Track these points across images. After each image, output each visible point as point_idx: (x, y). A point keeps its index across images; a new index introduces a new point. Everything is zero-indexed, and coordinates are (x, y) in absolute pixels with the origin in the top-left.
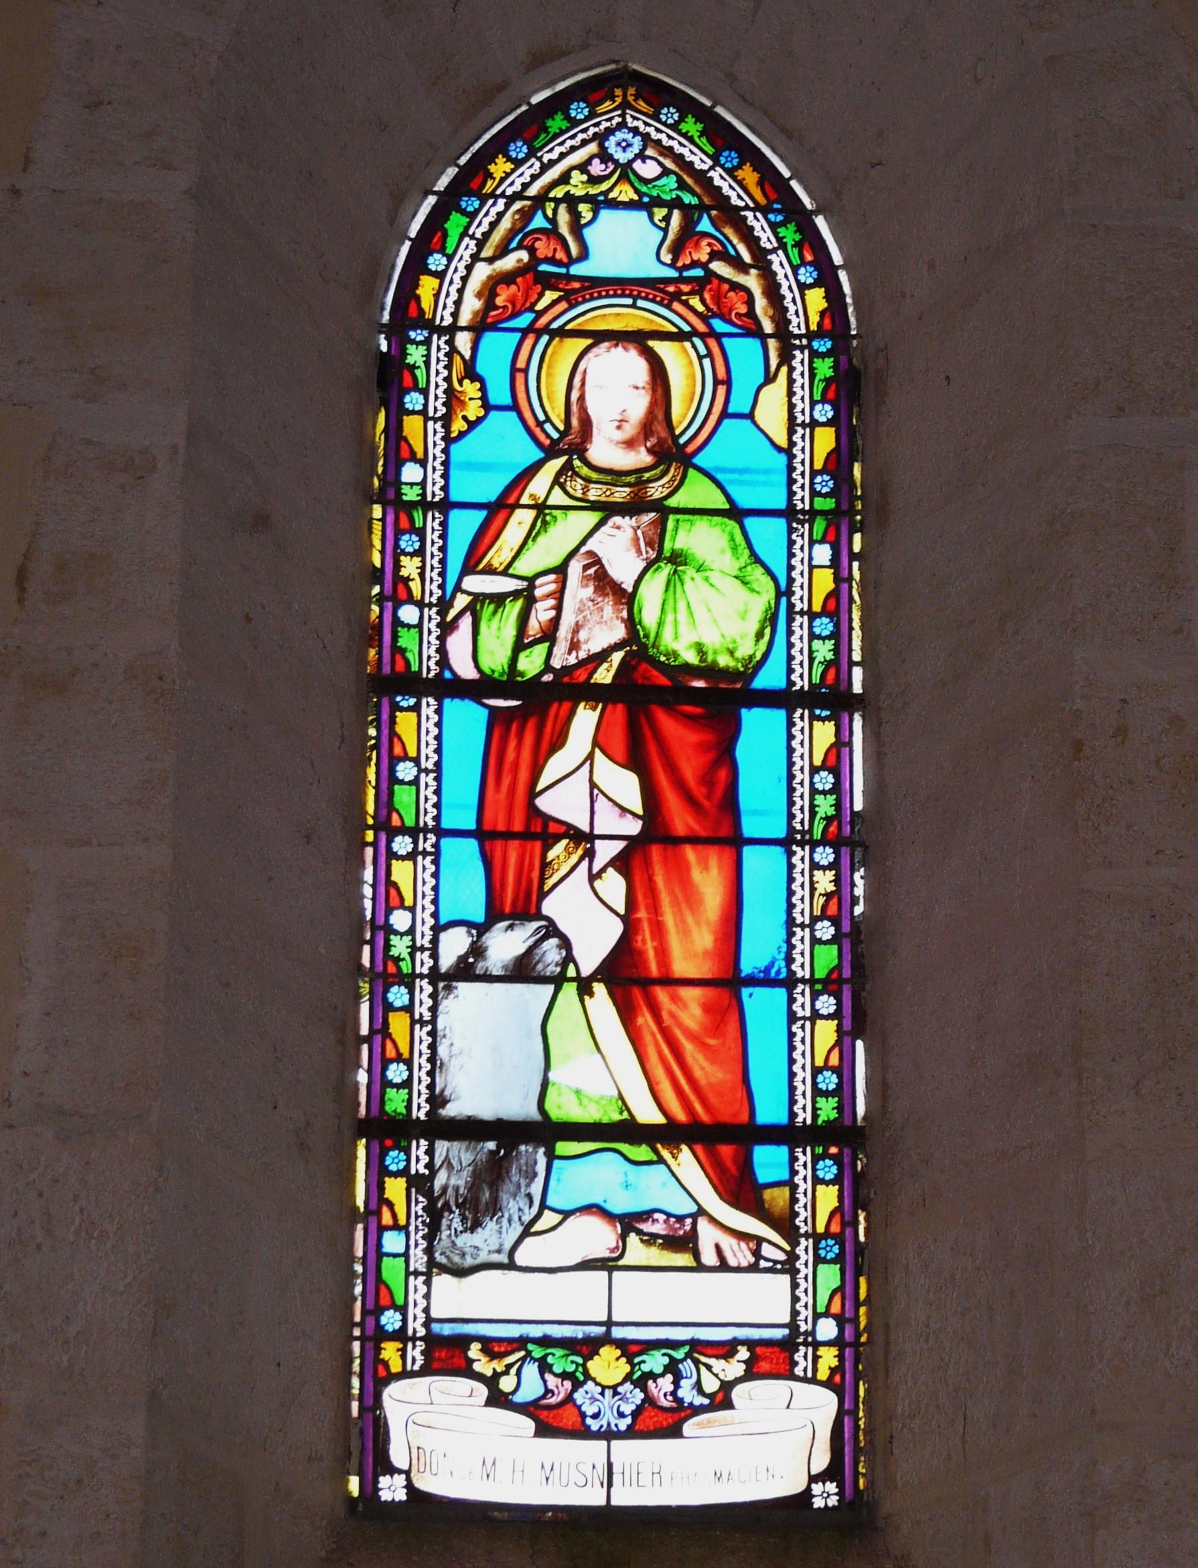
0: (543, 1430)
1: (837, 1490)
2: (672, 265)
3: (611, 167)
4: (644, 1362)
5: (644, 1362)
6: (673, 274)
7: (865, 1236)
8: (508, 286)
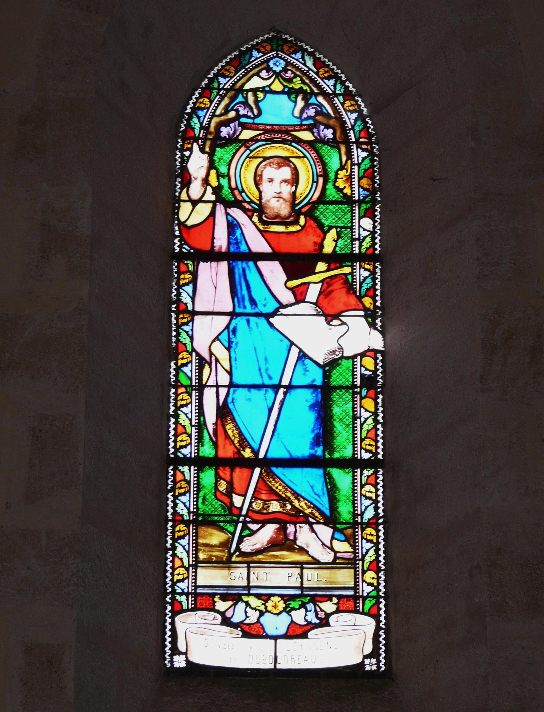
0: (246, 635)
5: (290, 604)
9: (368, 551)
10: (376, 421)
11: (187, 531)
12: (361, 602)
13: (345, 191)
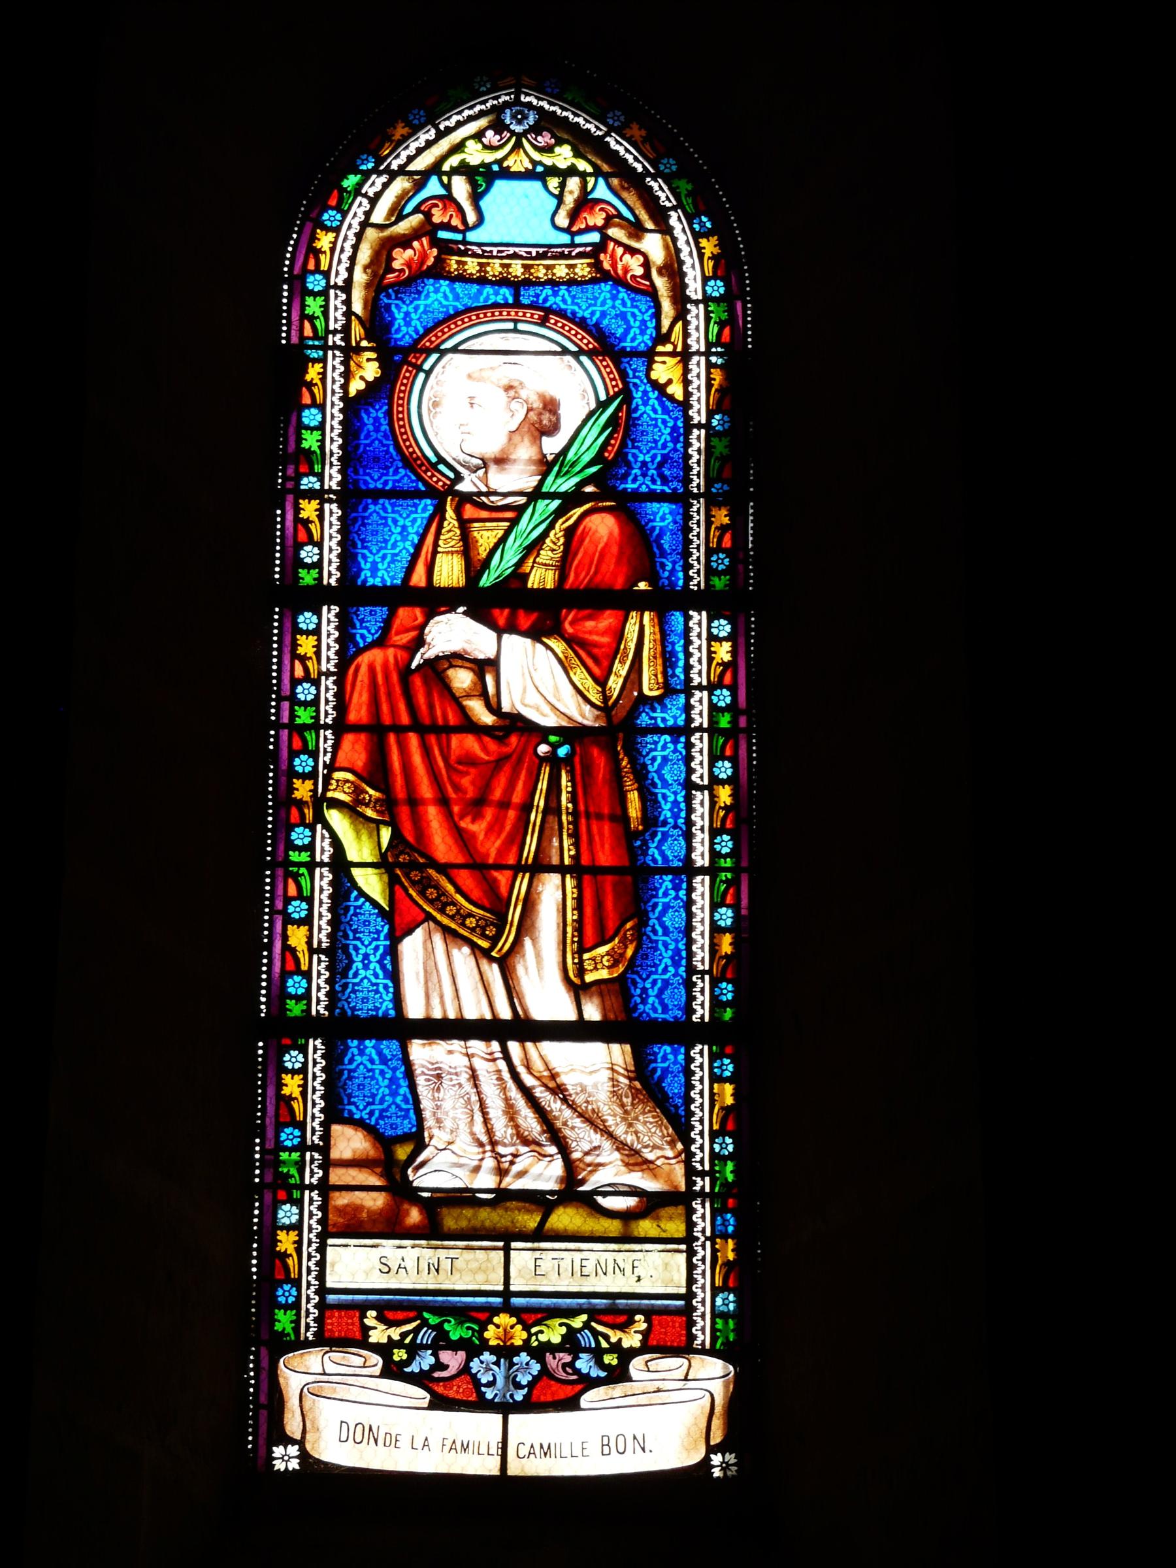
0: (439, 1403)
1: (291, 1469)
2: (567, 230)
4: (542, 1332)
6: (565, 239)
8: (405, 249)
11: (298, 1178)
13: (670, 390)
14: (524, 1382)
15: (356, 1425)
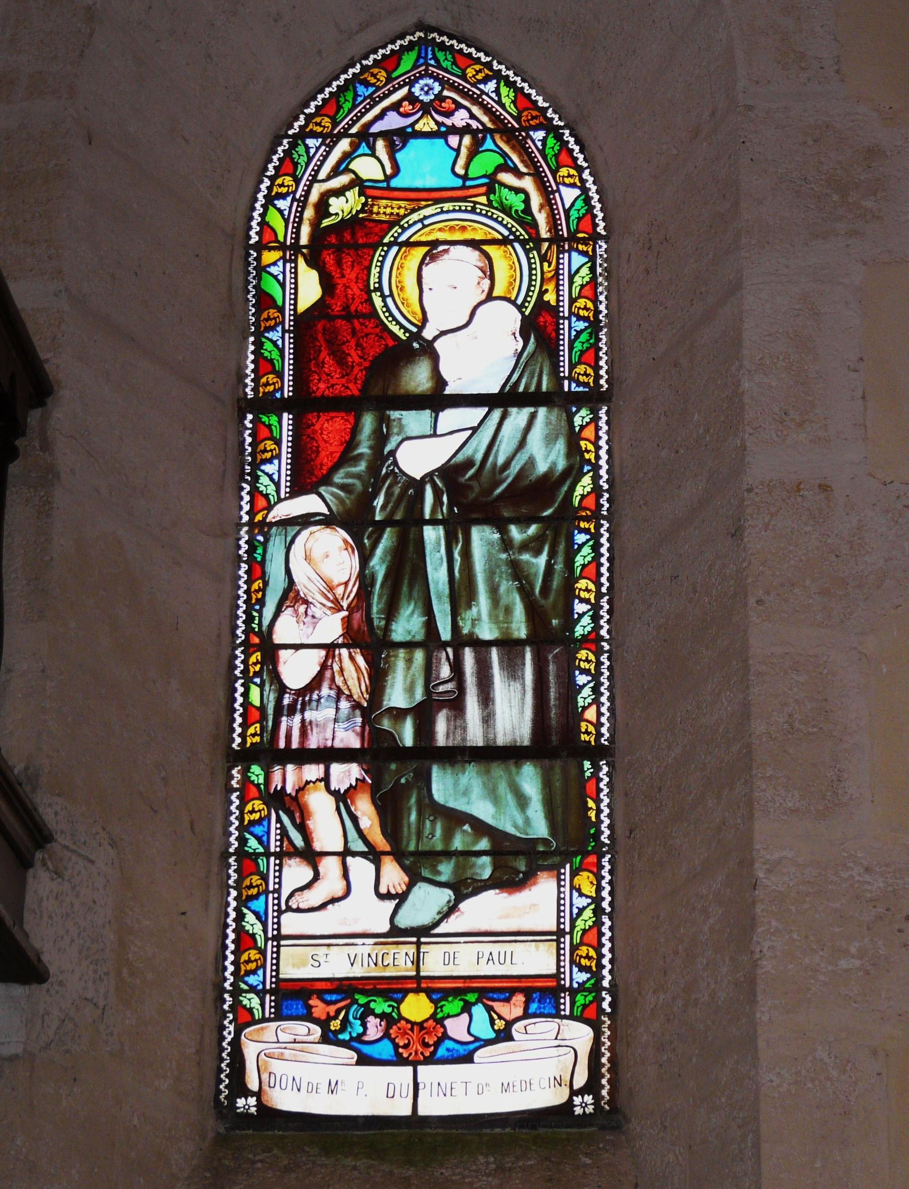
0: (364, 1060)
1: (575, 1109)
3: (418, 106)
7: (280, 722)
9: (581, 911)
10: (598, 912)
12: (568, 998)
14: (431, 1042)
15: (393, 1097)
